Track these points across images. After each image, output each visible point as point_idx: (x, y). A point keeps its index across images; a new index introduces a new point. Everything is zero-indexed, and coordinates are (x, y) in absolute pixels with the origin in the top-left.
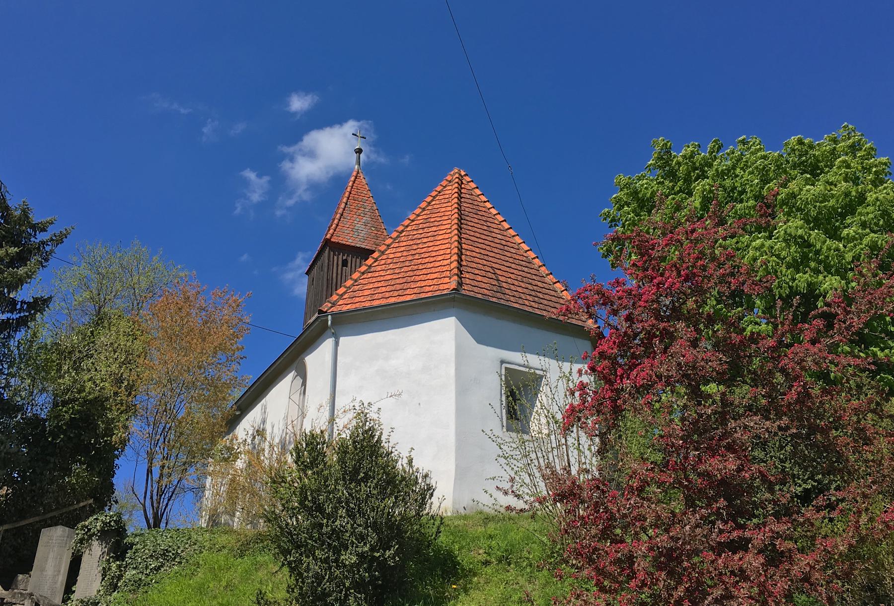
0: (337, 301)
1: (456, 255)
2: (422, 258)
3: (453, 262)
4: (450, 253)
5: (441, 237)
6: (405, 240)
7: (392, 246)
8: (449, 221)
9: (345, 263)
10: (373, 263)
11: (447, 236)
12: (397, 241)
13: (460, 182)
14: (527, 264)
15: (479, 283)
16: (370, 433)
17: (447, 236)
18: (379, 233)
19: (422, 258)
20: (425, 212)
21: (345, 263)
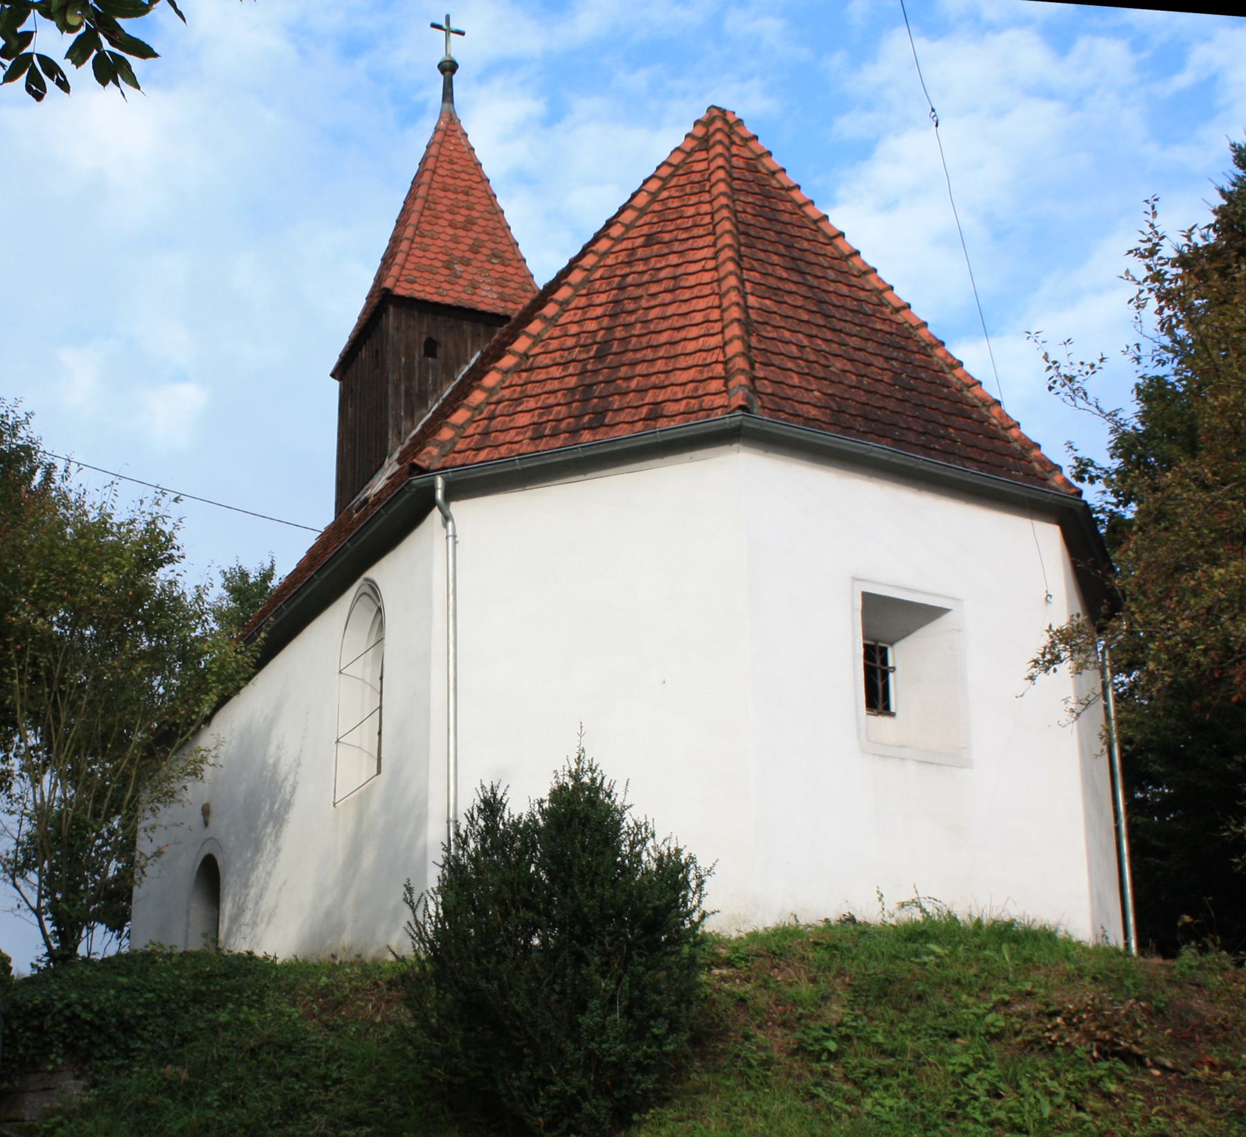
0: (453, 442)
1: (735, 324)
2: (693, 238)
3: (731, 340)
4: (721, 320)
5: (691, 346)
6: (604, 288)
7: (572, 305)
8: (709, 240)
9: (431, 348)
10: (529, 349)
11: (706, 277)
12: (584, 292)
13: (726, 141)
14: (781, 285)
15: (795, 391)
16: (595, 788)
17: (706, 277)
18: (510, 270)
19: (693, 238)
20: (647, 219)
21: (431, 348)
